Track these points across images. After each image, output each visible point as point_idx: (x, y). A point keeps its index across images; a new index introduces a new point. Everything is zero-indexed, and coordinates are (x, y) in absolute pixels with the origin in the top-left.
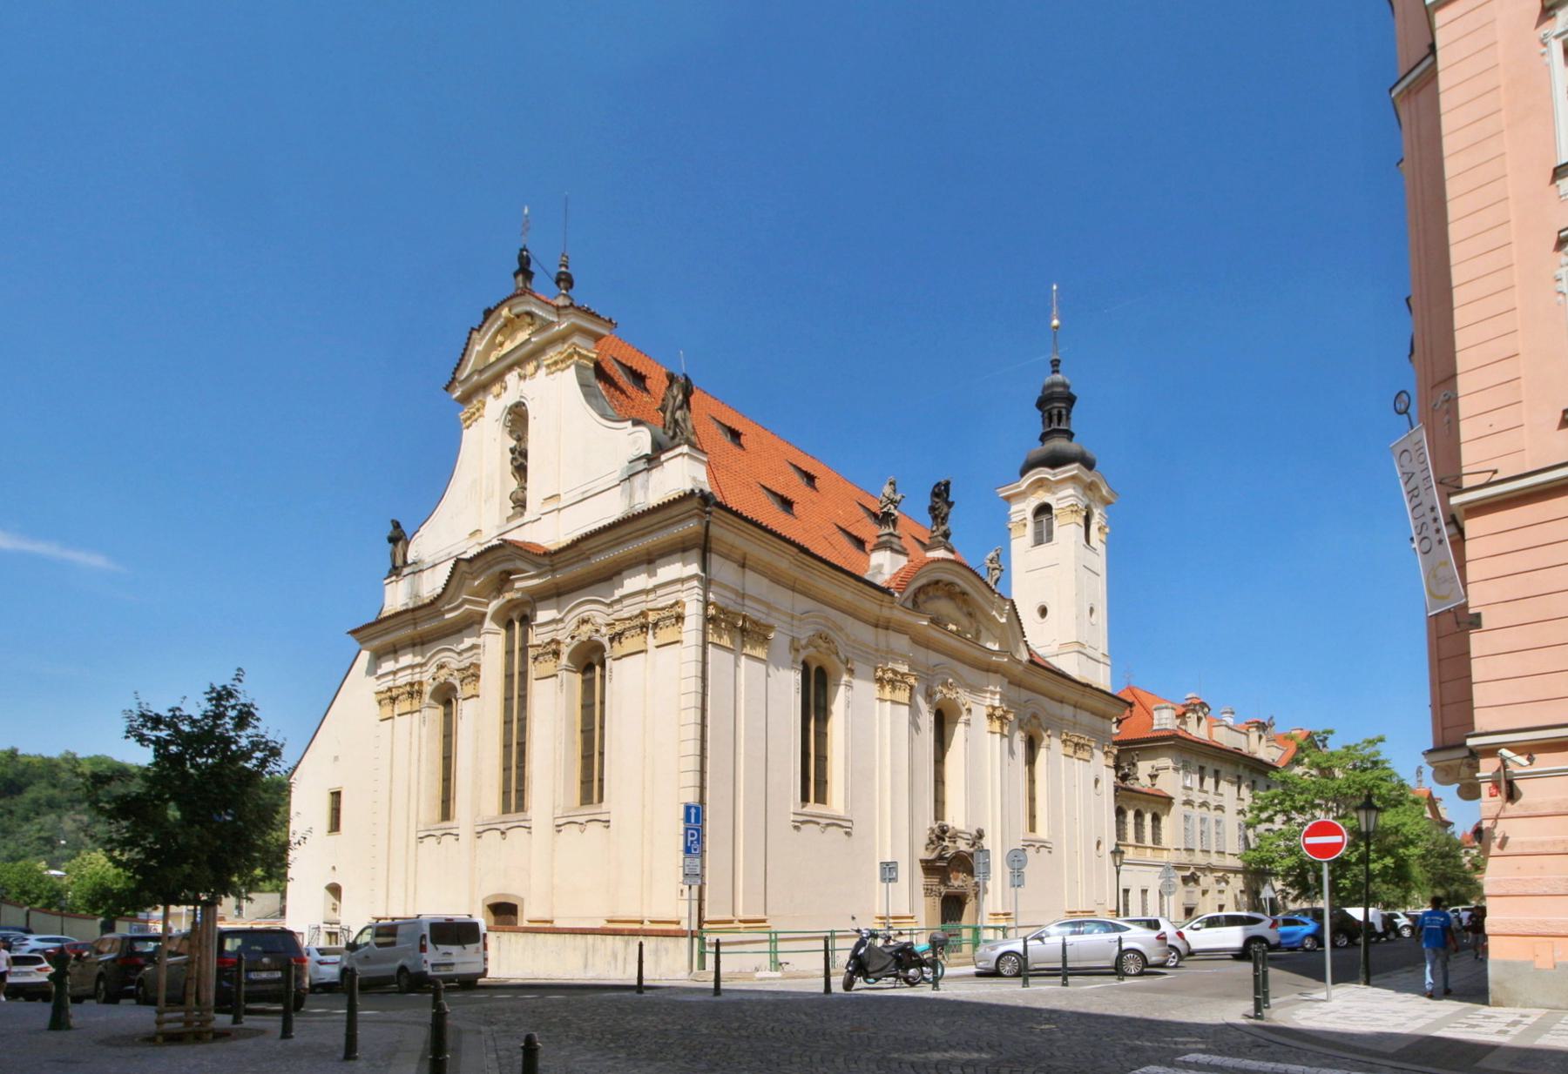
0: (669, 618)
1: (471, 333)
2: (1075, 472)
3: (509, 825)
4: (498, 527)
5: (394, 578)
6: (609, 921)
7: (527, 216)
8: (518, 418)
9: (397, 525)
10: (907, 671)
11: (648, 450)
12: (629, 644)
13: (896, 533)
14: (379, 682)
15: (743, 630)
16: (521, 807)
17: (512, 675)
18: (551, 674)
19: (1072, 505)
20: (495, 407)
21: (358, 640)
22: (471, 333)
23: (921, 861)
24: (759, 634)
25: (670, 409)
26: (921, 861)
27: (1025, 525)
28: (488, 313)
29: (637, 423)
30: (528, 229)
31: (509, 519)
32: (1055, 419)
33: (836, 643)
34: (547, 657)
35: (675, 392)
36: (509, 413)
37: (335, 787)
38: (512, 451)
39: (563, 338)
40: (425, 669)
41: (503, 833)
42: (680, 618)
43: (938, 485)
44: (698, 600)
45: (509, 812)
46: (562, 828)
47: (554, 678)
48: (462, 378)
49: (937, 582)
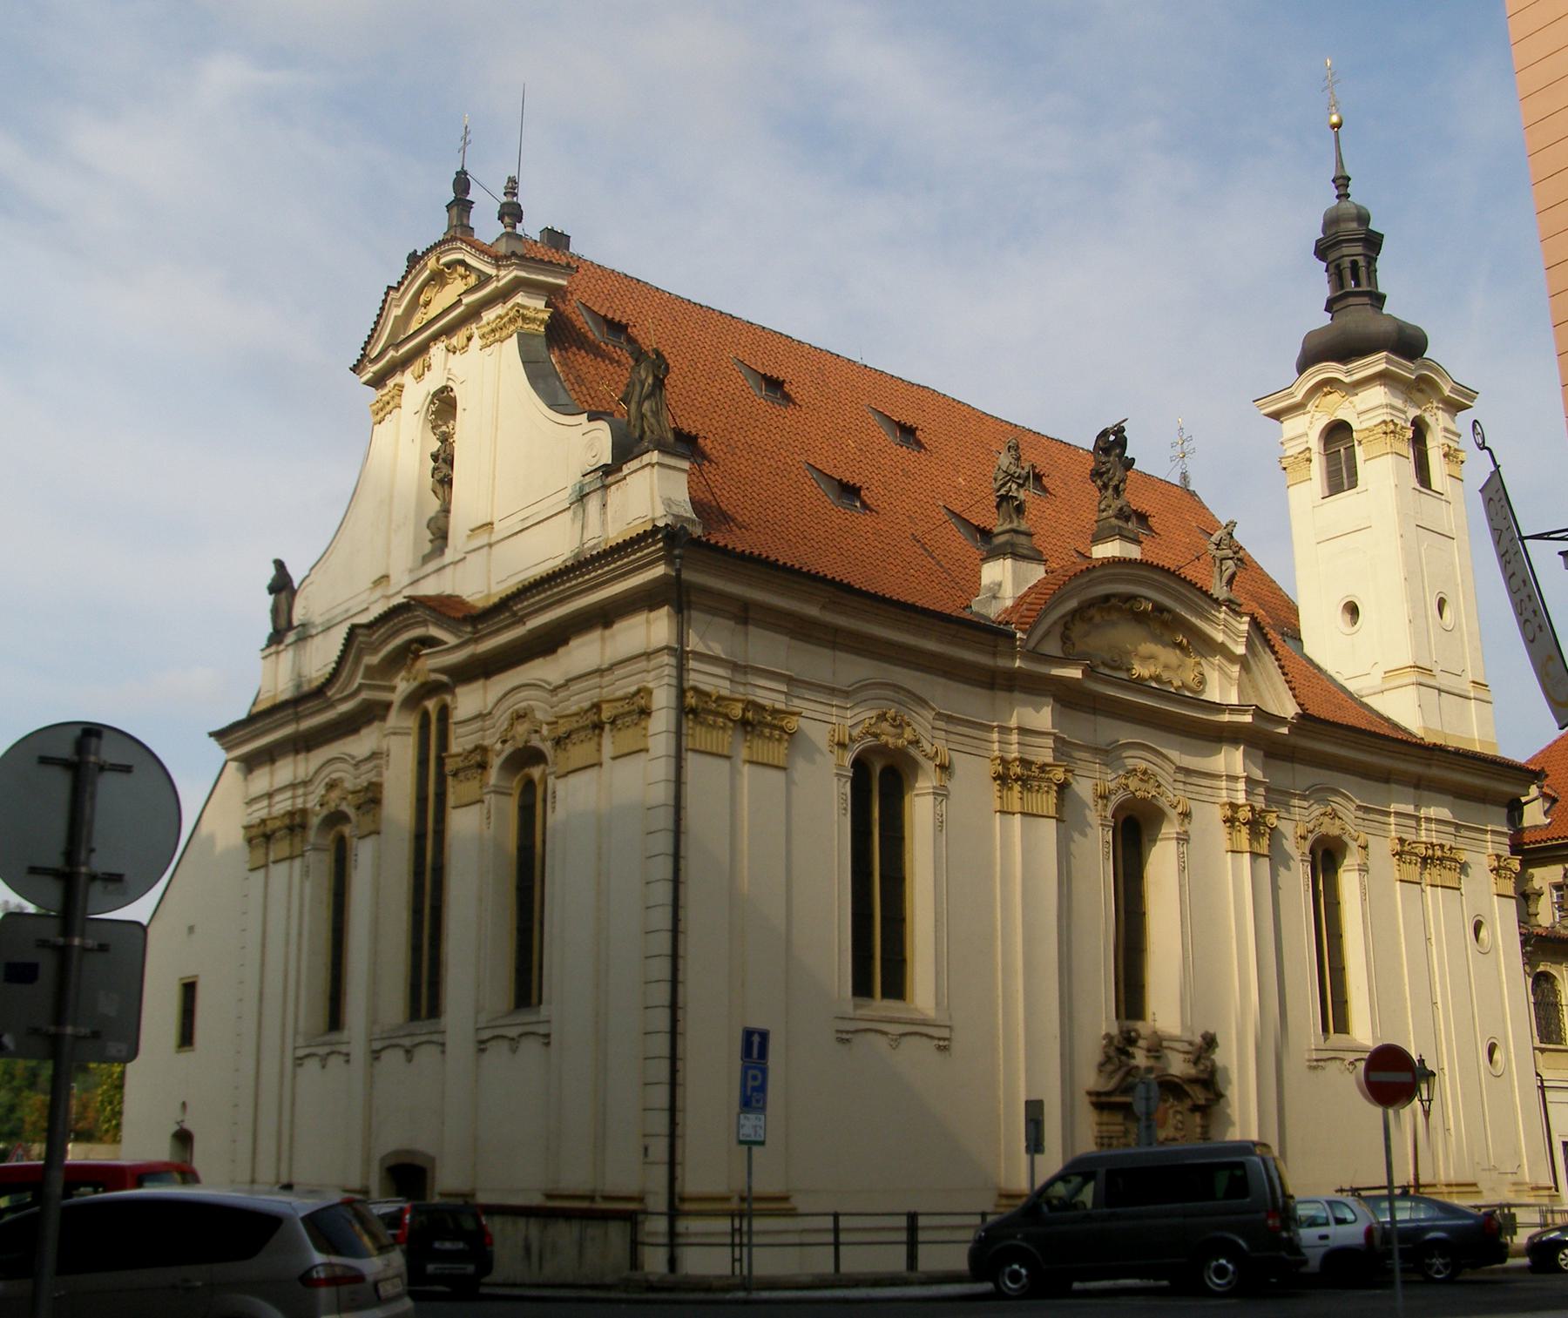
0: (629, 713)
1: (387, 294)
2: (1382, 366)
3: (417, 1040)
4: (411, 571)
5: (273, 649)
6: (549, 1196)
8: (444, 405)
10: (1050, 760)
11: (607, 458)
12: (579, 752)
13: (1024, 526)
14: (250, 811)
15: (744, 724)
16: (435, 1010)
18: (473, 799)
19: (1384, 422)
21: (222, 745)
23: (1089, 1093)
24: (774, 727)
25: (635, 398)
26: (1089, 1093)
27: (1309, 460)
31: (426, 559)
32: (1347, 273)
34: (469, 773)
35: (643, 375)
36: (432, 402)
37: (188, 972)
38: (435, 457)
39: (503, 295)
40: (311, 788)
41: (409, 1052)
42: (645, 712)
43: (1104, 434)
44: (669, 685)
46: (488, 1045)
47: (478, 806)
48: (372, 357)
49: (1107, 598)
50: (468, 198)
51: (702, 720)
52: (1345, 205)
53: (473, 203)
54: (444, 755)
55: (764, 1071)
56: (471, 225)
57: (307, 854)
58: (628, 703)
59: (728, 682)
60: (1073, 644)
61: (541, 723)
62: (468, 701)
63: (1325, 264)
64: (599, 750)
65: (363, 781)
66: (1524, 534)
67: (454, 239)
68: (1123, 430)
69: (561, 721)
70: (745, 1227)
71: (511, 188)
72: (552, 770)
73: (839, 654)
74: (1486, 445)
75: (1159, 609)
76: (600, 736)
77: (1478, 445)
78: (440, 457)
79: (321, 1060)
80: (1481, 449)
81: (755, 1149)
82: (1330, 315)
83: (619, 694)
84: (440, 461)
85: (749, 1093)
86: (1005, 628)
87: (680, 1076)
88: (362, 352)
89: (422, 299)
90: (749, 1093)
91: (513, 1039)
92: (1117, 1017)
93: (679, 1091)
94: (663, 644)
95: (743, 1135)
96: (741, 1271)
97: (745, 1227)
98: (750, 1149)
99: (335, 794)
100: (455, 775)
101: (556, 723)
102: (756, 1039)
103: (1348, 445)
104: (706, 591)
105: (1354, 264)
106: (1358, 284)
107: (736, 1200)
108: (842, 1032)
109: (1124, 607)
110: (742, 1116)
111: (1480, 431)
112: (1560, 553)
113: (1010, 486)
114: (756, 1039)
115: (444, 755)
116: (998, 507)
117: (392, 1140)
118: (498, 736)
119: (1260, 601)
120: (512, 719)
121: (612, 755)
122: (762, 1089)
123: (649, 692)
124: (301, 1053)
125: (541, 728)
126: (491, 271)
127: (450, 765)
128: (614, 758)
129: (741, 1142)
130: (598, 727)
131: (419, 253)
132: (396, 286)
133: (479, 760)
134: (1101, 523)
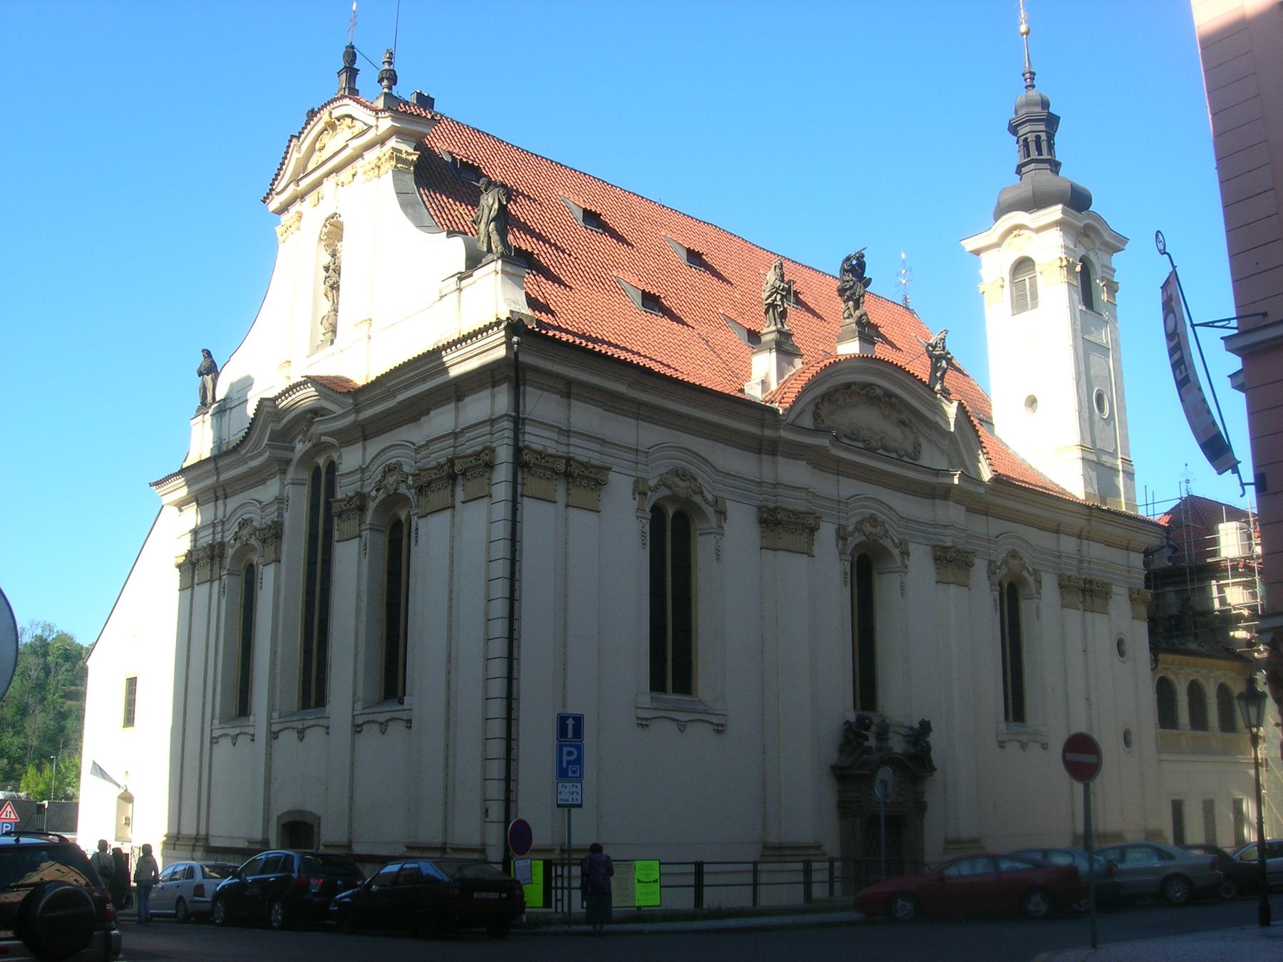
7: (354, 12)
8: (334, 231)
9: (208, 354)
12: (437, 497)
16: (321, 701)
17: (317, 535)
20: (312, 214)
22: (290, 141)
28: (312, 114)
29: (451, 233)
30: (355, 24)
33: (700, 480)
42: (490, 466)
43: (848, 259)
45: (309, 707)
49: (848, 386)
50: (355, 67)
51: (533, 472)
52: (1033, 93)
53: (359, 70)
54: (331, 500)
55: (580, 749)
56: (357, 88)
57: (224, 578)
58: (476, 459)
59: (554, 443)
60: (823, 420)
61: (407, 475)
62: (350, 459)
63: (1016, 138)
64: (453, 496)
65: (268, 520)
66: (1194, 323)
67: (343, 97)
68: (863, 256)
69: (422, 473)
70: (566, 873)
71: (389, 58)
72: (415, 512)
73: (641, 423)
74: (1166, 251)
75: (889, 395)
76: (454, 485)
77: (1160, 251)
78: (331, 268)
79: (232, 739)
80: (1163, 254)
81: (574, 811)
82: (1019, 177)
83: (469, 451)
84: (331, 271)
85: (565, 765)
86: (771, 405)
87: (514, 753)
88: (271, 187)
89: (318, 146)
90: (565, 765)
91: (381, 724)
92: (855, 708)
93: (513, 764)
94: (504, 412)
95: (561, 800)
96: (563, 909)
97: (566, 873)
98: (569, 811)
99: (245, 532)
100: (340, 516)
101: (419, 475)
102: (570, 722)
103: (1032, 276)
104: (536, 370)
105: (1038, 138)
106: (1040, 153)
107: (557, 851)
108: (642, 719)
109: (861, 392)
110: (560, 785)
111: (1162, 240)
112: (1222, 338)
113: (776, 297)
114: (570, 722)
115: (331, 500)
116: (767, 312)
117: (285, 803)
118: (373, 485)
119: (962, 394)
120: (385, 472)
121: (462, 499)
122: (579, 761)
123: (493, 450)
124: (216, 733)
125: (407, 479)
126: (371, 120)
127: (336, 508)
128: (463, 502)
129: (559, 806)
130: (453, 478)
131: (316, 110)
132: (297, 135)
133: (359, 503)
134: (845, 328)
